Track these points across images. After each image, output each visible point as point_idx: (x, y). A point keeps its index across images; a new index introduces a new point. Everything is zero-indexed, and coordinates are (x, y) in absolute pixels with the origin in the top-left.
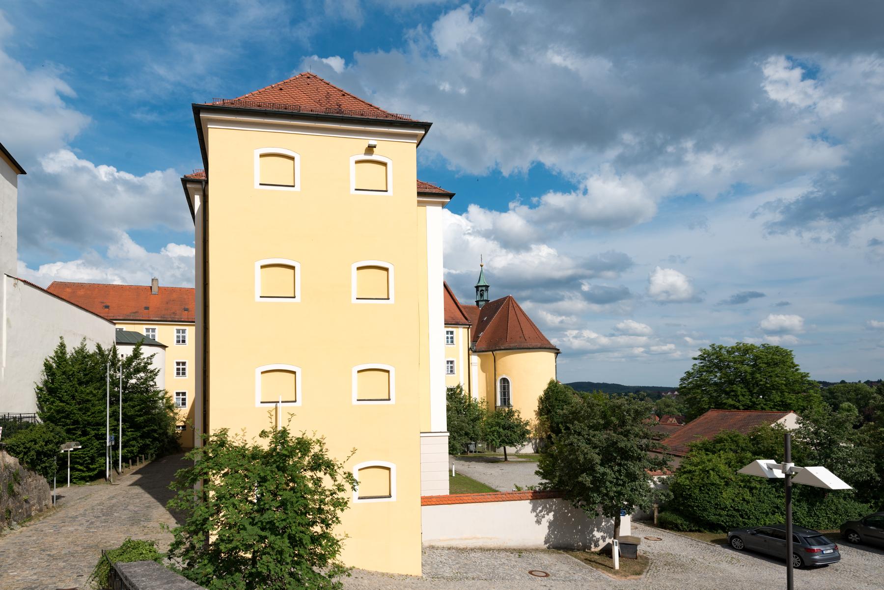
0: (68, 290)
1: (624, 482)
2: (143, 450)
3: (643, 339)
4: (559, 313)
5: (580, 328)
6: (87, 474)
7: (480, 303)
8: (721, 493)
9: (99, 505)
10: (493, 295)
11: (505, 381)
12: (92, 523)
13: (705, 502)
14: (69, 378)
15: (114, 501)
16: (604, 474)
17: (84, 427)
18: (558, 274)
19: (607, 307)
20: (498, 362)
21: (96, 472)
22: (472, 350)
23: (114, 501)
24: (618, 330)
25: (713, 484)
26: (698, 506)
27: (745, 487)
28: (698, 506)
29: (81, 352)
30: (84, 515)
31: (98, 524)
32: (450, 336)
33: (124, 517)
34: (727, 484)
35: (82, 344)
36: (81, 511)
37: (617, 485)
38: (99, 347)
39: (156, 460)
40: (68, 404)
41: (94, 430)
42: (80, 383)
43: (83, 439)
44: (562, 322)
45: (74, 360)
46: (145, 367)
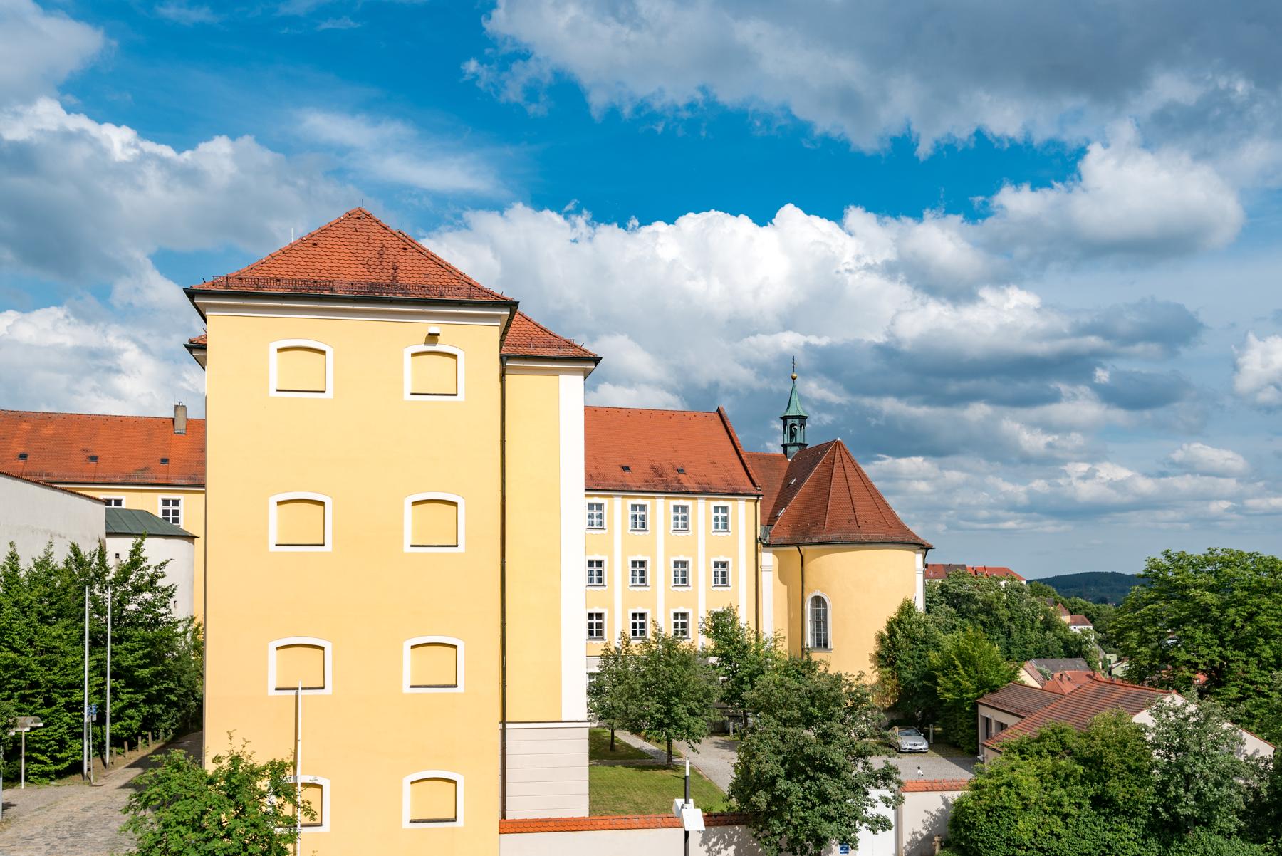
0: (26, 426)
1: (814, 805)
2: (149, 723)
3: (1230, 485)
4: (1048, 427)
5: (1094, 456)
6: (53, 768)
7: (790, 449)
8: (1016, 821)
9: (66, 819)
10: (811, 437)
11: (819, 601)
12: (54, 847)
13: (993, 836)
14: (24, 612)
15: (91, 814)
16: (788, 793)
17: (48, 692)
18: (1042, 348)
19: (1147, 414)
20: (807, 566)
21: (66, 765)
22: (763, 543)
23: (91, 814)
24: (1173, 463)
25: (1005, 808)
26: (983, 842)
27: (1053, 812)
28: (983, 842)
29: (43, 564)
30: (43, 835)
31: (62, 848)
32: (720, 515)
33: (100, 839)
34: (1025, 808)
35: (46, 551)
36: (40, 828)
37: (804, 808)
38: (75, 549)
39: (174, 739)
40: (23, 654)
41: (63, 696)
42: (43, 619)
43: (46, 711)
44: (1050, 445)
45: (33, 578)
46: (152, 582)
